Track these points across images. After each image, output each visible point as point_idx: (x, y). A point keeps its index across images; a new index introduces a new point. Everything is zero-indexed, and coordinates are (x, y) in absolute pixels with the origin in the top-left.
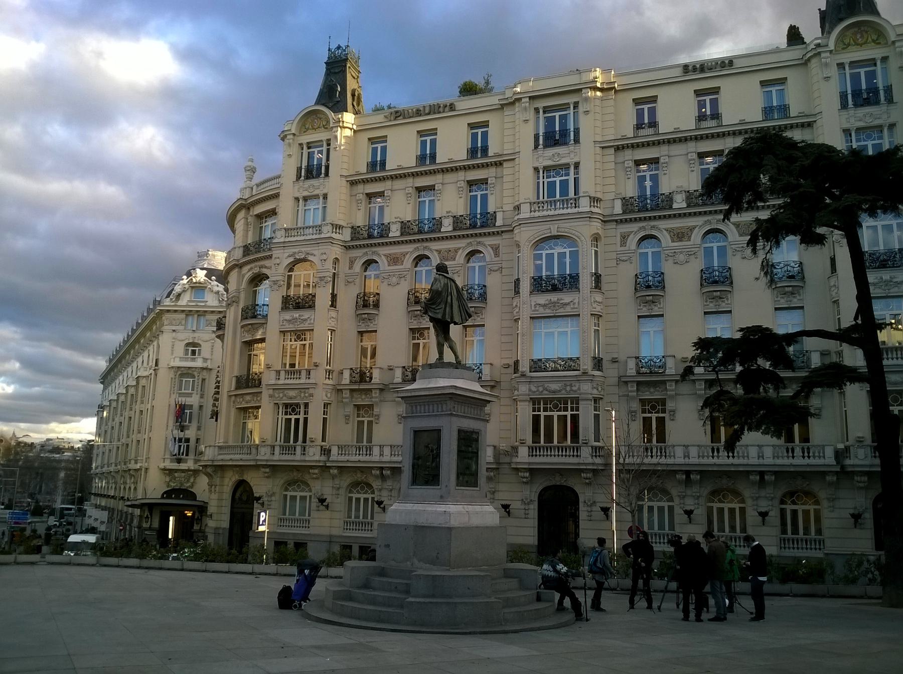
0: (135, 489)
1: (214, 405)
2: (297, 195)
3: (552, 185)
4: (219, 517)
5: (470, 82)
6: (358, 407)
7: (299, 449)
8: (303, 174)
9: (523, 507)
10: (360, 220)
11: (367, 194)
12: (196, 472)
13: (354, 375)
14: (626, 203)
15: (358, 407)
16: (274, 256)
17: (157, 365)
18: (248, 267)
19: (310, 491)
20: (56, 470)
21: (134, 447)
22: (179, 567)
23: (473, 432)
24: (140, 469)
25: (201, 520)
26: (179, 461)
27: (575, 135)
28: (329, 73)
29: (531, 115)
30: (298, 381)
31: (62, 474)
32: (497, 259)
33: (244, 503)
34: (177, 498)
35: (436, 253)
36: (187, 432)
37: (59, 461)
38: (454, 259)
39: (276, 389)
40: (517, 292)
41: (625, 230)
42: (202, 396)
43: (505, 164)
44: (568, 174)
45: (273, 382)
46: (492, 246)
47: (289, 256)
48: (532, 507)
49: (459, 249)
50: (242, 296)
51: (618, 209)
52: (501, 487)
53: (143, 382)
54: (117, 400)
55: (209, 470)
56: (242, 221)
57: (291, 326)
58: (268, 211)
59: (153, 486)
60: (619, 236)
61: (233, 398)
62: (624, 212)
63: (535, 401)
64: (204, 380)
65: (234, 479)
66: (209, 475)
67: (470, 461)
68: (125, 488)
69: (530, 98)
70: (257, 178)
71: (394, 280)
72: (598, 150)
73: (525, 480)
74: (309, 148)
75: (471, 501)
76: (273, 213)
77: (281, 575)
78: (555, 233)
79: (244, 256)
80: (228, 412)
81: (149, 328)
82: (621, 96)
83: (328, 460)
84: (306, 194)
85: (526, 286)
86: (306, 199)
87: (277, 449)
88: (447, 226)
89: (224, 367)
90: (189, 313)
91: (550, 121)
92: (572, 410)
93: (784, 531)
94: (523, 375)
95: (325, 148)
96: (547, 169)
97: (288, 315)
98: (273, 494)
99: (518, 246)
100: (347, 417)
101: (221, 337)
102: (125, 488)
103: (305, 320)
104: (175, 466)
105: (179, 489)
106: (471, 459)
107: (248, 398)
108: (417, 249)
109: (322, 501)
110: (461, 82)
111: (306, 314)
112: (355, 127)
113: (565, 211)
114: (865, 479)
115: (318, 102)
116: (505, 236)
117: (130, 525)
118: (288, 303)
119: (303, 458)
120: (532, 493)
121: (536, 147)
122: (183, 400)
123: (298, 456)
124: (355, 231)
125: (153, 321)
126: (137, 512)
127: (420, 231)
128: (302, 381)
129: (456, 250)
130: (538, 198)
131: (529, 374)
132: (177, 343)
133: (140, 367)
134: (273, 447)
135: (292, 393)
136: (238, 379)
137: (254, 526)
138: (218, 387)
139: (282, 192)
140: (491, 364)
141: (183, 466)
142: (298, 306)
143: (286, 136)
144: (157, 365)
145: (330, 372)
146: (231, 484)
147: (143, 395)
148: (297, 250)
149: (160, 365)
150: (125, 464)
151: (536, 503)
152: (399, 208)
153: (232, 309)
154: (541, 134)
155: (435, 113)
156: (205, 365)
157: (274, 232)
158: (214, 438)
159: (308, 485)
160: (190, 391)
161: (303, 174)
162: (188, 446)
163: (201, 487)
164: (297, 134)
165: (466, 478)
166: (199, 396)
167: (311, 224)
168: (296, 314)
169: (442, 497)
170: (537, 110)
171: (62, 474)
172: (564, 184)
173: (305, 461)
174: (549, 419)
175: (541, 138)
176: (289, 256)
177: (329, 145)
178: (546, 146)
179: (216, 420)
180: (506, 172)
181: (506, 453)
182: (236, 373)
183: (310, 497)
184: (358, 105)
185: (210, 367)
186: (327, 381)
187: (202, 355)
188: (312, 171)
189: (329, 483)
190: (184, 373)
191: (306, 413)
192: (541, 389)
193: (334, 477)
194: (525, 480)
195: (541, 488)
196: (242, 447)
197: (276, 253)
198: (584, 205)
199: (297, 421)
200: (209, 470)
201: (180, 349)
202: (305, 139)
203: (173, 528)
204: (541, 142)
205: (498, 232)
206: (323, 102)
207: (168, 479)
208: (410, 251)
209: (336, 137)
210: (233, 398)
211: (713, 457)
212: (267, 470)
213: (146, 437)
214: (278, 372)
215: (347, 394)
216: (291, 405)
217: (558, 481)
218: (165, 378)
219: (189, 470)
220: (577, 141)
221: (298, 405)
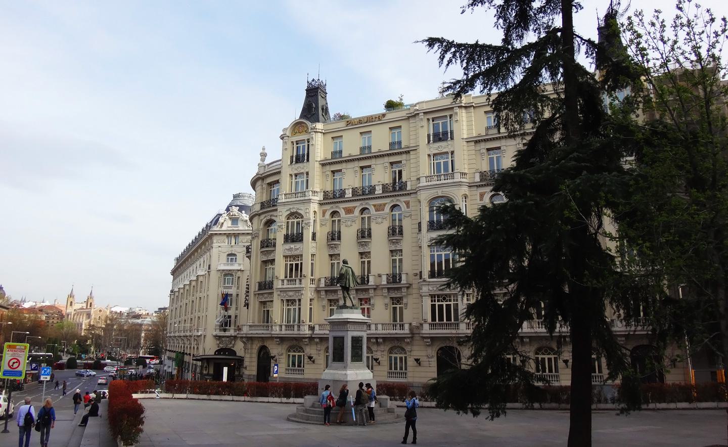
0: (198, 348)
1: (246, 300)
2: (291, 173)
3: (439, 164)
4: (251, 368)
5: (391, 101)
6: (330, 301)
7: (296, 327)
8: (294, 160)
9: (428, 360)
10: (329, 188)
11: (332, 171)
12: (235, 337)
13: (327, 281)
14: (483, 175)
15: (330, 301)
16: (278, 210)
17: (209, 268)
18: (264, 215)
19: (304, 352)
20: (140, 331)
21: (196, 321)
22: (232, 399)
23: (359, 337)
24: (201, 335)
25: (240, 368)
26: (225, 330)
27: (451, 135)
28: (308, 96)
29: (425, 123)
30: (294, 286)
31: (143, 335)
32: (408, 210)
33: (265, 360)
34: (224, 354)
35: (372, 206)
36: (229, 311)
37: (141, 325)
38: (384, 210)
39: (283, 291)
40: (420, 230)
41: (482, 191)
42: (238, 288)
43: (411, 153)
44: (448, 158)
45: (280, 286)
46: (405, 202)
47: (287, 211)
48: (433, 360)
49: (387, 203)
50: (261, 233)
51: (477, 179)
52: (415, 348)
53: (201, 279)
54: (184, 288)
55: (244, 340)
56: (260, 187)
57: (290, 252)
58: (275, 181)
59: (209, 347)
60: (478, 195)
61: (257, 296)
62: (481, 180)
63: (432, 296)
64: (239, 278)
65: (259, 345)
66: (244, 343)
67: (358, 350)
68: (190, 348)
69: (424, 113)
70: (267, 161)
71: (349, 223)
72: (465, 143)
73: (428, 344)
74: (297, 144)
75: (359, 368)
76: (277, 182)
78: (440, 194)
79: (261, 209)
80: (254, 304)
81: (204, 243)
82: (477, 110)
83: (313, 334)
84: (296, 172)
85: (424, 227)
86: (296, 175)
87: (284, 327)
88: (379, 191)
89: (251, 276)
90: (228, 235)
91: (435, 127)
92: (454, 301)
93: (391, 368)
94: (424, 281)
95: (306, 144)
96: (435, 155)
97: (288, 246)
98: (282, 354)
99: (420, 202)
100: (324, 306)
101: (249, 257)
102: (190, 348)
103: (298, 249)
104: (222, 334)
105: (226, 348)
106: (358, 349)
107: (266, 295)
108: (362, 204)
109: (310, 358)
110: (385, 102)
111: (298, 245)
112: (323, 131)
113: (446, 181)
114: (429, 340)
115: (301, 117)
116: (412, 196)
117: (185, 368)
118: (289, 239)
119: (298, 332)
120: (433, 352)
121: (429, 142)
122: (226, 291)
123: (296, 332)
124: (326, 195)
125: (207, 240)
126: (199, 363)
127: (365, 193)
128: (297, 286)
129: (385, 205)
130: (431, 173)
131: (428, 280)
132: (222, 254)
133: (198, 269)
134: (281, 326)
135: (291, 293)
136: (260, 284)
137: (271, 375)
138: (248, 288)
139: (283, 171)
140: (407, 274)
141: (227, 334)
142: (293, 241)
143: (283, 137)
144: (209, 268)
145: (312, 280)
146: (257, 348)
147: (201, 288)
148: (291, 207)
149: (212, 267)
150: (190, 332)
151: (435, 359)
152: (350, 180)
153: (255, 241)
154: (431, 134)
155: (370, 122)
156: (239, 268)
157: (278, 196)
158: (247, 318)
159: (302, 348)
160: (231, 285)
161: (294, 160)
162: (230, 320)
163: (239, 348)
164: (290, 136)
165: (356, 358)
166: (236, 288)
167: (300, 191)
168: (292, 246)
169: (345, 367)
170: (428, 120)
171: (143, 335)
172: (446, 164)
173: (300, 334)
174: (441, 307)
175: (431, 137)
176: (287, 211)
177: (308, 142)
178: (434, 141)
179: (248, 308)
180: (412, 157)
181: (418, 328)
182: (258, 280)
183: (304, 355)
184: (326, 114)
185: (242, 269)
186: (312, 286)
187: (237, 262)
188: (300, 158)
189: (314, 347)
190: (227, 274)
191: (299, 305)
192: (435, 289)
193: (317, 344)
194: (428, 344)
195: (438, 348)
196: (263, 326)
197: (279, 208)
198: (458, 177)
199: (295, 309)
200: (244, 340)
201: (224, 257)
202: (295, 139)
203: (221, 373)
204: (431, 139)
205: (408, 194)
206: (305, 116)
207: (218, 342)
208: (358, 206)
209: (312, 138)
210: (257, 296)
211: (539, 328)
212: (278, 340)
213: (204, 314)
214: (283, 281)
215: (323, 293)
216: (291, 300)
217: (448, 344)
218: (215, 277)
219: (231, 336)
220: (452, 138)
221: (295, 300)
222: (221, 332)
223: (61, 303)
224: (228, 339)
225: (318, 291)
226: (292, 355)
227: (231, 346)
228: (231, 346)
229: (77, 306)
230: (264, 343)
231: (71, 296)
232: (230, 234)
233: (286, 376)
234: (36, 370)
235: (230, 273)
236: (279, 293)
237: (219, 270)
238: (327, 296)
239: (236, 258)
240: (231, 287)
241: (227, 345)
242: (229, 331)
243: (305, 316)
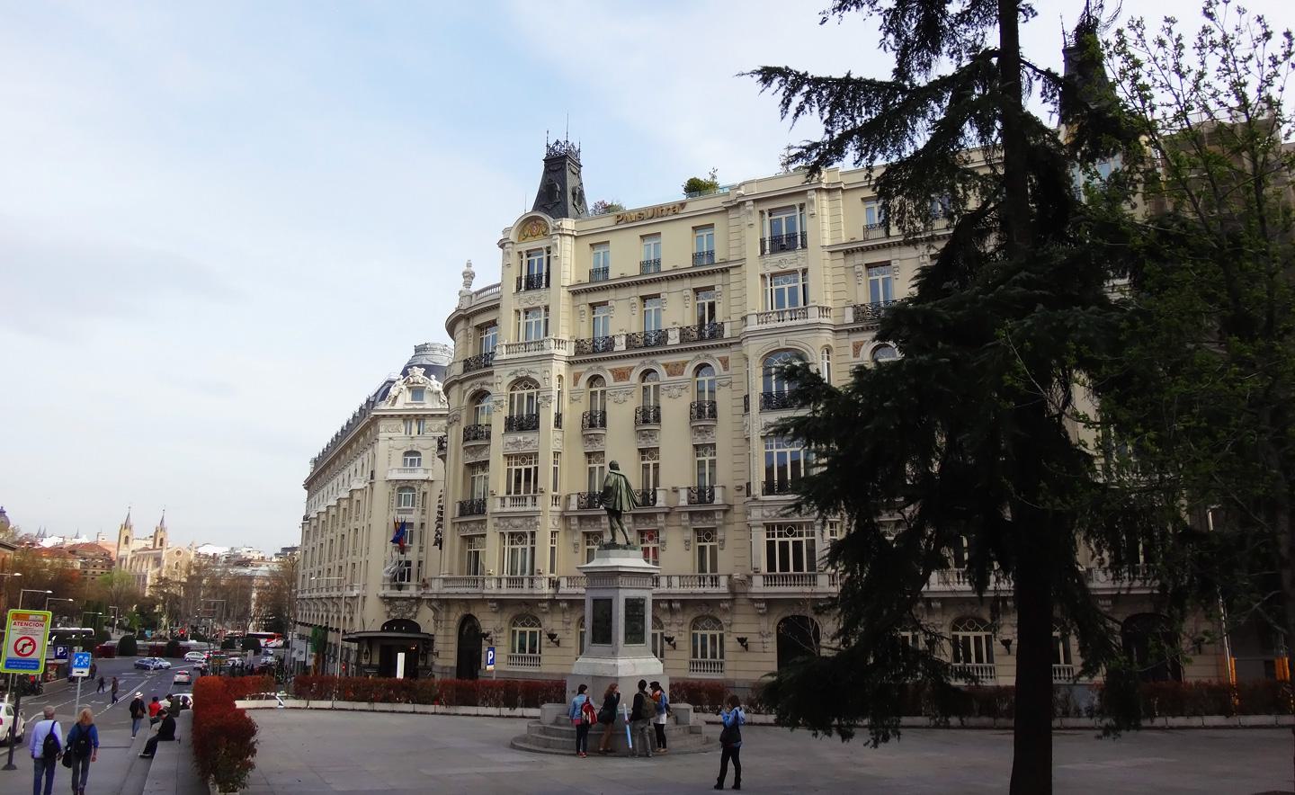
0: (351, 619)
1: (438, 533)
2: (518, 307)
3: (780, 292)
4: (446, 655)
5: (695, 179)
6: (587, 535)
7: (526, 582)
8: (523, 285)
9: (761, 640)
10: (585, 334)
11: (590, 304)
12: (418, 600)
13: (582, 500)
14: (858, 311)
15: (587, 535)
16: (495, 374)
17: (372, 477)
18: (470, 383)
19: (540, 626)
20: (249, 588)
21: (349, 572)
22: (412, 710)
23: (639, 599)
24: (357, 597)
25: (426, 655)
26: (400, 588)
27: (802, 239)
28: (548, 171)
29: (756, 219)
30: (522, 509)
31: (254, 595)
32: (726, 373)
33: (471, 641)
34: (399, 630)
35: (662, 367)
36: (408, 554)
37: (251, 578)
38: (682, 374)
39: (503, 517)
40: (747, 410)
41: (857, 340)
42: (423, 512)
43: (732, 271)
44: (796, 281)
45: (498, 509)
46: (720, 359)
47: (510, 374)
48: (769, 640)
49: (688, 362)
50: (464, 415)
51: (849, 318)
52: (738, 619)
53: (357, 496)
54: (327, 512)
55: (434, 604)
56: (462, 333)
57: (515, 449)
58: (489, 322)
59: (372, 618)
60: (851, 346)
61: (457, 526)
62: (856, 321)
63: (769, 527)
64: (425, 494)
65: (460, 614)
66: (434, 609)
67: (636, 623)
68: (338, 618)
69: (754, 201)
70: (476, 287)
71: (621, 397)
72: (827, 255)
73: (761, 611)
74: (528, 256)
75: (638, 655)
76: (493, 323)
77: (336, 709)
78: (783, 346)
79: (465, 372)
80: (453, 540)
81: (362, 432)
82: (849, 195)
83: (557, 593)
84: (527, 306)
85: (755, 403)
86: (527, 312)
87: (504, 582)
88: (674, 339)
89: (447, 491)
90: (406, 419)
91: (775, 226)
92: (807, 535)
93: (695, 655)
94: (755, 499)
95: (545, 256)
96: (773, 275)
97: (512, 438)
98: (501, 630)
99: (747, 359)
100: (576, 545)
101: (443, 458)
102: (338, 618)
103: (530, 443)
104: (395, 593)
105: (402, 620)
106: (637, 621)
107: (472, 525)
108: (643, 363)
109: (552, 636)
110: (685, 181)
111: (530, 436)
112: (575, 233)
113: (794, 323)
114: (763, 605)
115: (536, 208)
116: (734, 348)
117: (328, 654)
118: (514, 425)
119: (530, 591)
120: (770, 626)
121: (763, 252)
122: (402, 517)
123: (526, 590)
124: (580, 347)
125: (367, 427)
126: (354, 646)
127: (649, 343)
128: (528, 509)
129: (684, 364)
130: (767, 308)
131: (762, 498)
132: (394, 452)
133: (352, 479)
134: (500, 580)
135: (517, 522)
136: (462, 505)
137: (483, 667)
138: (441, 513)
139: (503, 304)
140: (724, 487)
141: (404, 593)
142: (521, 428)
143: (504, 244)
144: (372, 477)
145: (556, 498)
146: (457, 619)
147: (358, 512)
148: (518, 368)
149: (377, 476)
150: (338, 590)
151: (774, 638)
152: (623, 320)
153: (454, 428)
154: (767, 239)
155: (658, 217)
156: (425, 477)
157: (495, 348)
158: (440, 566)
159: (537, 620)
160: (410, 507)
161: (523, 285)
162: (409, 570)
163: (425, 619)
164: (516, 242)
165: (633, 637)
166: (419, 513)
167: (533, 339)
168: (520, 437)
169: (613, 653)
170: (762, 213)
171: (254, 595)
172: (793, 291)
173: (533, 595)
174: (784, 546)
175: (767, 243)
176: (510, 374)
177: (549, 252)
178: (773, 251)
179: (440, 548)
180: (733, 279)
181: (743, 582)
182: (460, 498)
183: (540, 632)
184: (580, 203)
185: (431, 479)
186: (554, 508)
187: (422, 466)
188: (533, 282)
189: (559, 617)
190: (405, 487)
191: (533, 542)
192: (774, 513)
193: (564, 611)
194: (761, 611)
195: (780, 619)
196: (469, 580)
197: (497, 371)
198: (814, 316)
199: (524, 550)
200: (434, 604)
201: (398, 458)
202: (525, 247)
203: (393, 663)
204: (767, 247)
205: (726, 344)
206: (543, 206)
207: (388, 609)
208: (637, 366)
209: (556, 245)
210: (457, 526)
211: (959, 583)
212: (495, 604)
213: (362, 559)
214: (503, 499)
215: (575, 521)
216: (517, 534)
217: (797, 611)
218: (382, 492)
219: (411, 598)
220: (804, 246)
221: (524, 534)
222: (393, 591)
223: (109, 540)
224: (405, 603)
225: (565, 518)
226: (520, 632)
227: (411, 615)
228: (411, 615)
229: (136, 545)
230: (469, 610)
231: (127, 526)
232: (408, 415)
233: (509, 670)
234: (65, 657)
235: (409, 485)
236: (496, 520)
237: (390, 481)
238: (583, 526)
239: (419, 460)
240: (412, 510)
241: (403, 614)
242: (408, 589)
243: (543, 562)
